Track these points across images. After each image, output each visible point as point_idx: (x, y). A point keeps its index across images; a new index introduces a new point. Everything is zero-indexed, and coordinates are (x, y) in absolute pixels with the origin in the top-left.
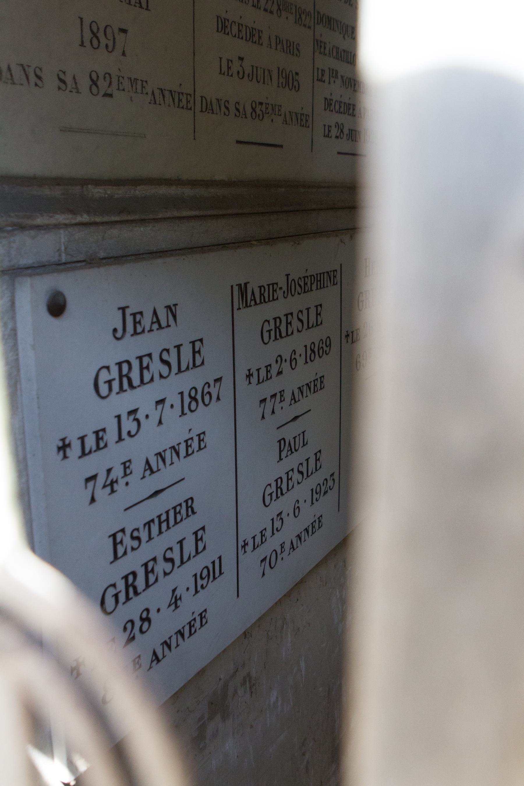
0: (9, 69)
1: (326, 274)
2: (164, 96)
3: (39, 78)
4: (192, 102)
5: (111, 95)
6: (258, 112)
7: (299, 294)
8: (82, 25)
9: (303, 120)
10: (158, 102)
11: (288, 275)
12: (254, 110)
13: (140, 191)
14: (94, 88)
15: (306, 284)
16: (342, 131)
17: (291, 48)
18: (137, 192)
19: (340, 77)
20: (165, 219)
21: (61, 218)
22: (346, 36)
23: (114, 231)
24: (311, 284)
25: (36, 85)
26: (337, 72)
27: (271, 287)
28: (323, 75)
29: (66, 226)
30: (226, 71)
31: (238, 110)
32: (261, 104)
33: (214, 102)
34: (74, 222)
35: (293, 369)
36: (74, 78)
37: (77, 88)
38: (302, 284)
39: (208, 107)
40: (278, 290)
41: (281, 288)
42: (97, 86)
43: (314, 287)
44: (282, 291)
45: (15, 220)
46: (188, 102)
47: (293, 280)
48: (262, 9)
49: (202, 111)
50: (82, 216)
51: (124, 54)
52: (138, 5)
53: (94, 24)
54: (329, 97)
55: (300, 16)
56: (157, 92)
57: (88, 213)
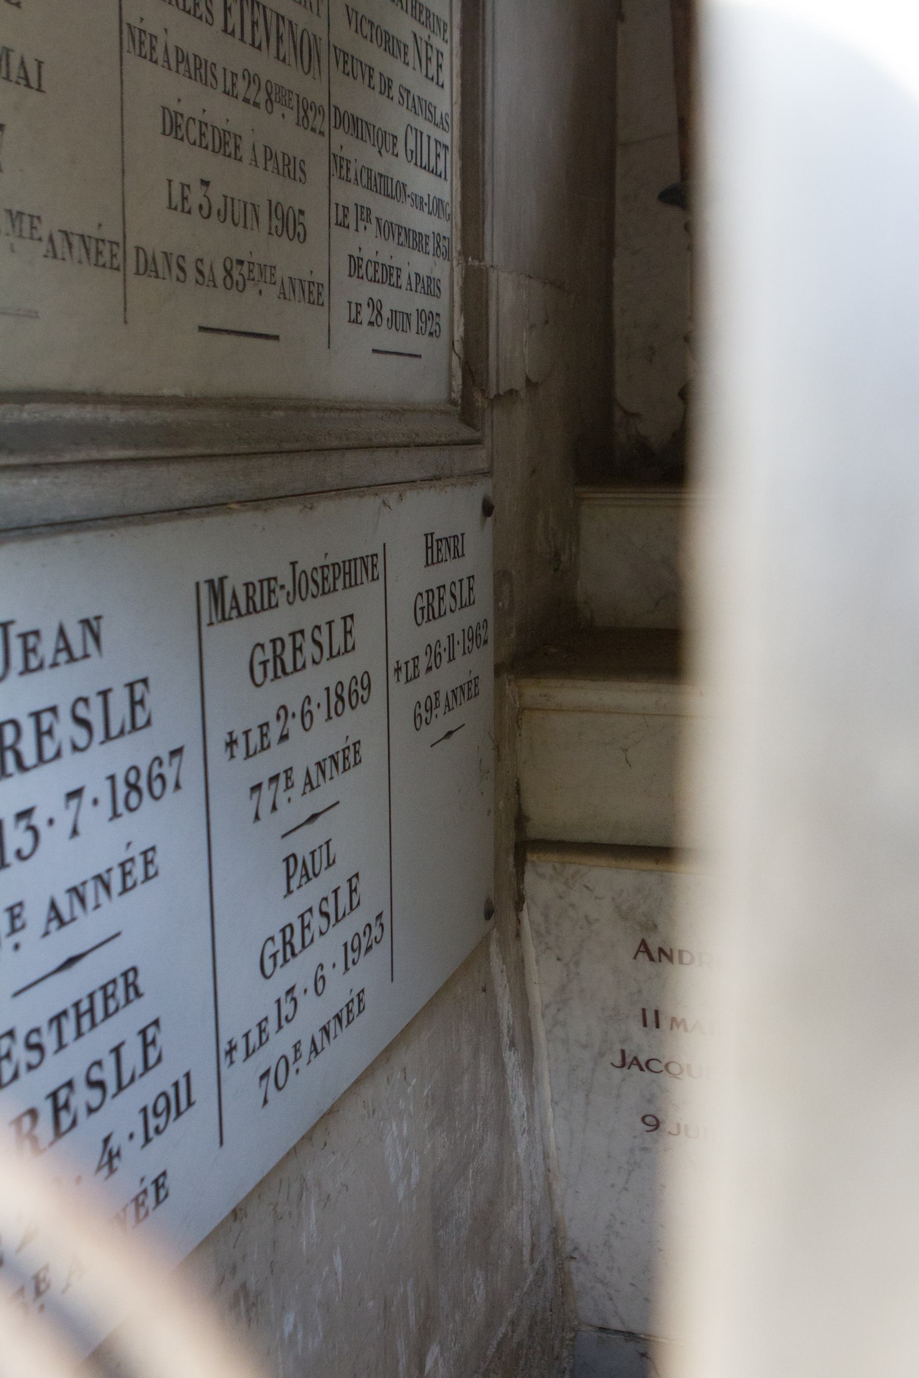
1: (358, 562)
2: (70, 245)
7: (313, 596)
9: (313, 293)
12: (229, 273)
15: (325, 579)
16: (379, 313)
19: (374, 221)
22: (383, 151)
24: (335, 579)
30: (180, 204)
31: (200, 272)
33: (160, 258)
39: (148, 267)
40: (277, 589)
41: (282, 587)
44: (285, 591)
47: (304, 572)
56: (58, 239)
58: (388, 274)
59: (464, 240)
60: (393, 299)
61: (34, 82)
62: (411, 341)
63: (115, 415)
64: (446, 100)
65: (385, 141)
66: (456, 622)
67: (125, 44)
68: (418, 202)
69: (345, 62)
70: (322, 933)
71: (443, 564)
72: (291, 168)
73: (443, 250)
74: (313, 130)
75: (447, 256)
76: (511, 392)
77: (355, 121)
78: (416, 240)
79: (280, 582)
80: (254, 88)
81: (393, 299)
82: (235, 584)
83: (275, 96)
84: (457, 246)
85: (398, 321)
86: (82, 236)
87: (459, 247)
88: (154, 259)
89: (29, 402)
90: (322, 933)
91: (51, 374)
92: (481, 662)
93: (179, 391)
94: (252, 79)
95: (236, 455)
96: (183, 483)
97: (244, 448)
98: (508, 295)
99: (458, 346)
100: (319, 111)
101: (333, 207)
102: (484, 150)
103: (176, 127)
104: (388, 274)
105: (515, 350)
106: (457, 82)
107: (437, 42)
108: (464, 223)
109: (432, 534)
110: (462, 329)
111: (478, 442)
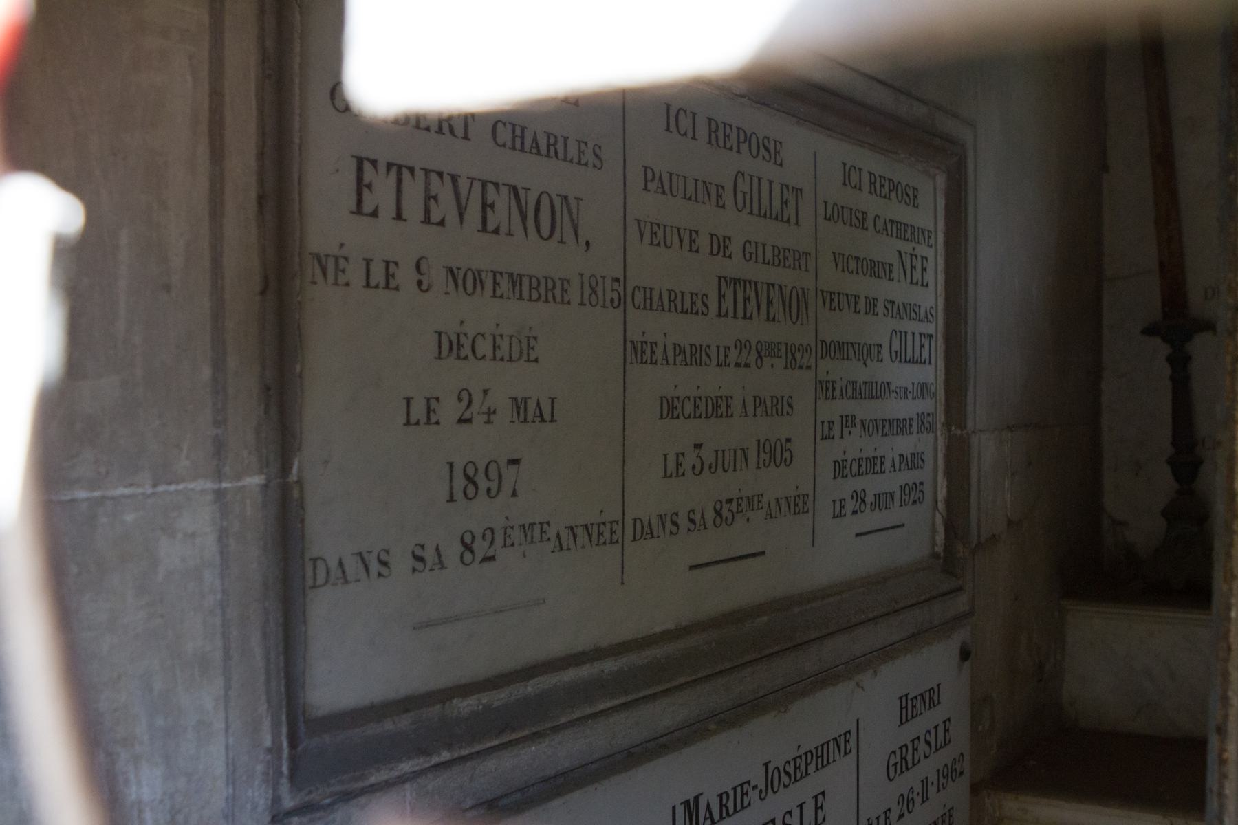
0: (341, 564)
1: (831, 744)
2: (575, 537)
3: (384, 564)
4: (619, 532)
5: (492, 558)
6: (725, 513)
7: (785, 786)
8: (451, 471)
9: (798, 504)
10: (565, 547)
11: (766, 765)
12: (718, 513)
13: (532, 687)
14: (468, 556)
15: (797, 768)
16: (863, 501)
17: (779, 406)
18: (529, 689)
19: (858, 424)
20: (572, 724)
21: (406, 767)
22: (868, 362)
23: (490, 764)
24: (807, 764)
25: (380, 575)
26: (854, 416)
27: (739, 789)
28: (830, 429)
29: (416, 775)
30: (675, 470)
31: (692, 521)
32: (730, 501)
33: (655, 522)
34: (427, 765)
35: (891, 780)
36: (437, 549)
37: (441, 562)
38: (791, 771)
39: (644, 531)
40: (750, 791)
41: (755, 787)
42: (472, 552)
43: (812, 768)
44: (757, 791)
45: (338, 788)
46: (612, 532)
47: (777, 768)
48: (732, 365)
49: (635, 540)
50: (439, 755)
51: (514, 494)
52: (534, 151)
53: (470, 465)
54: (840, 457)
55: (793, 355)
56: (565, 534)
57: (449, 747)
58: (873, 465)
59: (947, 412)
60: (873, 485)
61: (547, 417)
62: (896, 514)
63: (609, 666)
64: (931, 297)
65: (869, 352)
66: (929, 767)
67: (628, 357)
68: (903, 393)
69: (832, 300)
70: (926, 757)
71: (918, 718)
72: (779, 406)
73: (927, 425)
74: (801, 367)
75: (932, 428)
76: (994, 538)
77: (841, 346)
78: (899, 426)
79: (753, 784)
80: (745, 352)
81: (873, 485)
82: (710, 797)
83: (765, 351)
84: (941, 418)
85: (882, 501)
86: (586, 526)
87: (943, 420)
88: (650, 524)
89: (532, 677)
90: (926, 757)
91: (556, 646)
92: (957, 793)
93: (670, 626)
94: (742, 345)
95: (720, 672)
96: (666, 714)
97: (727, 665)
98: (989, 451)
99: (941, 506)
100: (806, 349)
101: (819, 424)
102: (966, 333)
103: (672, 408)
104: (873, 465)
105: (997, 495)
106: (941, 278)
107: (922, 250)
108: (947, 400)
109: (906, 695)
110: (945, 490)
111: (959, 589)
